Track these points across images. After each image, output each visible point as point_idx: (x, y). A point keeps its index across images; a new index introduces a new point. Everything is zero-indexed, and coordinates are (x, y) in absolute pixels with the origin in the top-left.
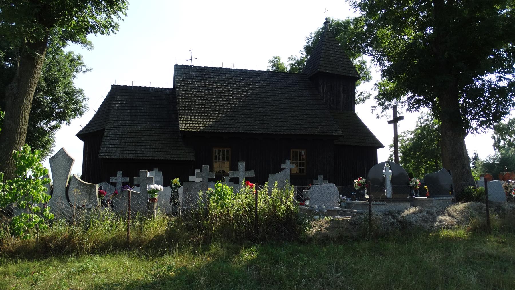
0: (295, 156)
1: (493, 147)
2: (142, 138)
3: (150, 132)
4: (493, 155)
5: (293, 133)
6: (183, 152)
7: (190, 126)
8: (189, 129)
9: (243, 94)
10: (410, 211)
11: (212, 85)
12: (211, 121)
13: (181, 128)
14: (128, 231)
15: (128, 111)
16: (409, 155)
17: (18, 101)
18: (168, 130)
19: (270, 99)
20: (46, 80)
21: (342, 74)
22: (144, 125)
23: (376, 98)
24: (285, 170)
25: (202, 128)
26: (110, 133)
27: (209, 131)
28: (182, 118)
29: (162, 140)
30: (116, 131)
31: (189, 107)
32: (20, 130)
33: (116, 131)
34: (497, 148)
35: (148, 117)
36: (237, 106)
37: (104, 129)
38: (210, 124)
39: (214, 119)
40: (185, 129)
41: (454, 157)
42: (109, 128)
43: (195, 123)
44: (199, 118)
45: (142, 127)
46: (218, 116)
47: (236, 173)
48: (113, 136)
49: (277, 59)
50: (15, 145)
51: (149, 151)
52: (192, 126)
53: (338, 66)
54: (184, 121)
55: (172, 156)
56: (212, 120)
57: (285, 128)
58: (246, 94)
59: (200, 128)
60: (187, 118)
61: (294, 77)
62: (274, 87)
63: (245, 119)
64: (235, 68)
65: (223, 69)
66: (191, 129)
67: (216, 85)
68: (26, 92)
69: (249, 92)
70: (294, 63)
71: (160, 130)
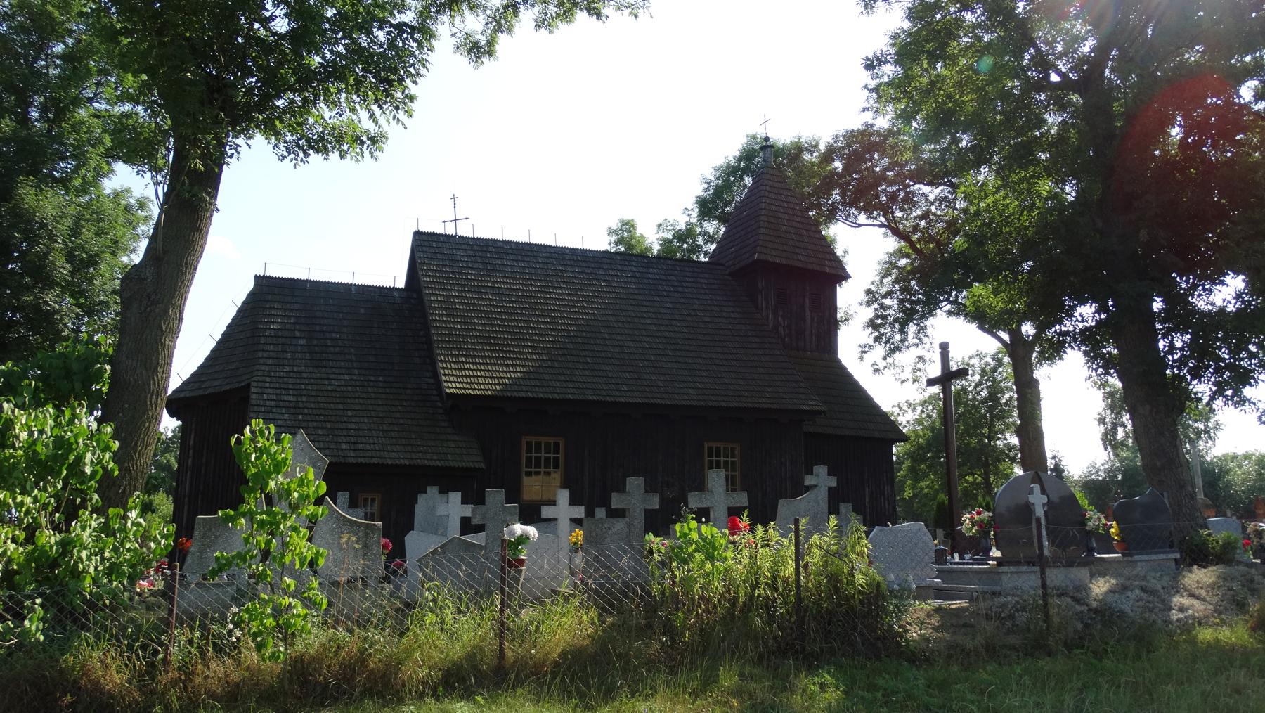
0: (552, 455)
1: (1101, 443)
2: (347, 410)
3: (365, 395)
4: (1103, 462)
5: (710, 404)
6: (453, 445)
7: (467, 383)
8: (468, 389)
9: (584, 307)
10: (1100, 587)
11: (510, 283)
12: (517, 372)
13: (449, 387)
14: (501, 637)
15: (303, 342)
16: (924, 460)
17: (157, 311)
18: (409, 391)
19: (649, 321)
20: (70, 257)
21: (810, 267)
22: (347, 377)
23: (867, 326)
24: (816, 491)
25: (498, 387)
26: (265, 396)
27: (516, 394)
28: (446, 362)
29: (398, 415)
30: (278, 391)
31: (459, 335)
32: (158, 383)
33: (278, 391)
34: (1110, 444)
35: (353, 358)
36: (574, 336)
37: (248, 386)
38: (515, 378)
39: (522, 366)
40: (458, 388)
41: (1158, 464)
42: (260, 384)
43: (479, 374)
44: (487, 364)
45: (343, 382)
46: (532, 360)
47: (705, 498)
48: (273, 403)
49: (629, 225)
50: (145, 423)
51: (370, 444)
52: (473, 383)
53: (800, 248)
54: (451, 369)
55: (428, 457)
56: (518, 369)
57: (691, 391)
58: (592, 308)
59: (494, 387)
60: (458, 363)
61: (696, 270)
62: (653, 293)
63: (596, 367)
64: (560, 244)
65: (530, 245)
66: (471, 389)
67: (519, 284)
68: (175, 291)
69: (597, 303)
70: (669, 235)
71: (388, 390)
